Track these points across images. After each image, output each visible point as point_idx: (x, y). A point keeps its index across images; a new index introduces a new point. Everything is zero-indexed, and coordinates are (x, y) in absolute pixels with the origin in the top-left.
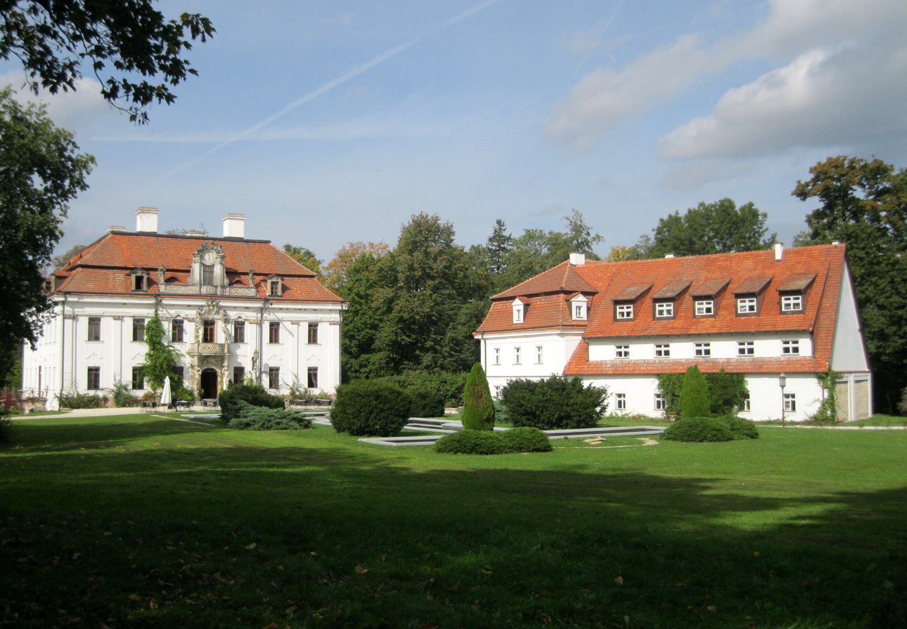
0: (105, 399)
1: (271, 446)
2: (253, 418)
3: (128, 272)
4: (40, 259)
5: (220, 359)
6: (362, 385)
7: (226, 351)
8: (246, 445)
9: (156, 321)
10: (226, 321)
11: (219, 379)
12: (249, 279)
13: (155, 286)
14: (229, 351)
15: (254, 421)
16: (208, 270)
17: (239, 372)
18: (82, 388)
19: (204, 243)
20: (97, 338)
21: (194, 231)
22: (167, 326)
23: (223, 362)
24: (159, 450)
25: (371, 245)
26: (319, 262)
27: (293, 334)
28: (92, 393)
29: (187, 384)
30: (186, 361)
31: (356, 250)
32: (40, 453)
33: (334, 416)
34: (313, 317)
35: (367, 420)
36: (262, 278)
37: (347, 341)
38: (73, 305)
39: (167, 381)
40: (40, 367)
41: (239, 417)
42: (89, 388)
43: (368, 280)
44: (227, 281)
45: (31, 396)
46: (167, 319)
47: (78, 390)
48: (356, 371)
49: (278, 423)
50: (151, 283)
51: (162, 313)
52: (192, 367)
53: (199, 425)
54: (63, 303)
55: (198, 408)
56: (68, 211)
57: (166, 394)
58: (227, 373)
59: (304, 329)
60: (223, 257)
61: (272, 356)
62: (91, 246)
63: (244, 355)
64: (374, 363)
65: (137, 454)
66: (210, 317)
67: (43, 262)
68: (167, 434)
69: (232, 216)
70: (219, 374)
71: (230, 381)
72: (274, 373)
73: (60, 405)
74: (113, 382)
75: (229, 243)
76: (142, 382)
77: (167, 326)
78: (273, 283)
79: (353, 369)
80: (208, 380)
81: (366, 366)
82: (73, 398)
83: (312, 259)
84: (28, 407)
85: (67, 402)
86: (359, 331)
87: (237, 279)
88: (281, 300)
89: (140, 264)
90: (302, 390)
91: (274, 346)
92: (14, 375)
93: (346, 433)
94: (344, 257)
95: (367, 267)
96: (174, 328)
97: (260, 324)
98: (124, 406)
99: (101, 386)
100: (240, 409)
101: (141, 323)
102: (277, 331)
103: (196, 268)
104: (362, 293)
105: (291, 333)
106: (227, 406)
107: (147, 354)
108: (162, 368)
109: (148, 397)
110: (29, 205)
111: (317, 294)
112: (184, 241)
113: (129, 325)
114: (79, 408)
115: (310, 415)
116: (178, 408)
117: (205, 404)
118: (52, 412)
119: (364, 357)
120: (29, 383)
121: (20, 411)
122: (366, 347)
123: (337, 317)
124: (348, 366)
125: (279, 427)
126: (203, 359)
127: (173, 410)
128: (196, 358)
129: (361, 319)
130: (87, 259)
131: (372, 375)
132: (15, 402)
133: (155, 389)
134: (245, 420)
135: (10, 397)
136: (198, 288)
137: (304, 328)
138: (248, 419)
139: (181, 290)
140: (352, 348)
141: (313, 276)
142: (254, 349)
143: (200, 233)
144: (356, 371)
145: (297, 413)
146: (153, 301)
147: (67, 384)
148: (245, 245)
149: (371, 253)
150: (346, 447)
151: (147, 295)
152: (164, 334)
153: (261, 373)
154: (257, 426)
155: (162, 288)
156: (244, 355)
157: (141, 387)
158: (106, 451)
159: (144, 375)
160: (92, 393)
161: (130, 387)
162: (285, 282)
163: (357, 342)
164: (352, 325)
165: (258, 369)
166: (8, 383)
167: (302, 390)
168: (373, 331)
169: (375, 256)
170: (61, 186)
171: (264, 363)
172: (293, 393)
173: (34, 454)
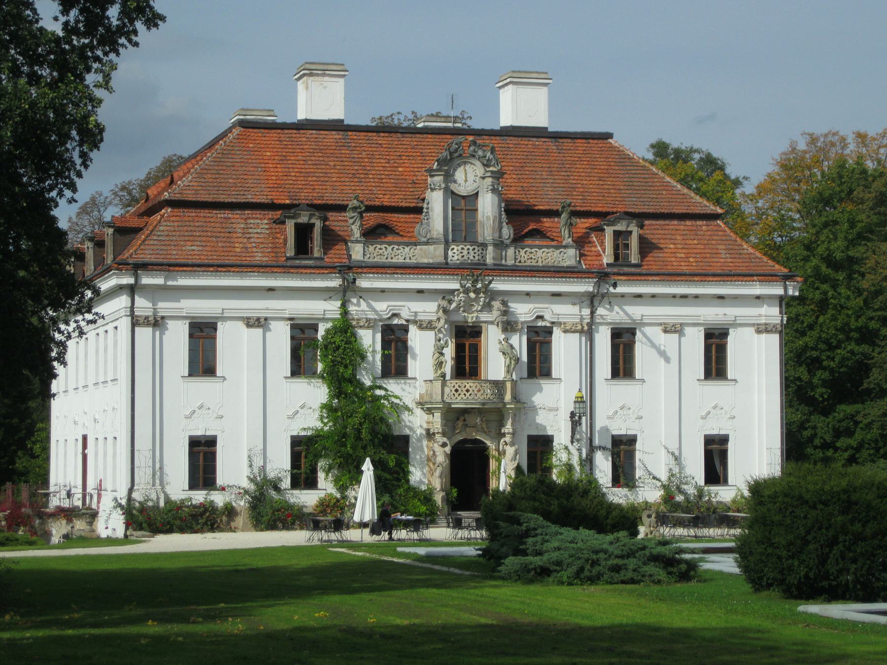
0: (230, 512)
1: (586, 623)
2: (555, 555)
3: (278, 214)
4: (51, 188)
5: (493, 415)
6: (836, 476)
7: (508, 397)
8: (527, 620)
9: (345, 328)
10: (509, 326)
11: (493, 464)
12: (559, 225)
13: (340, 246)
14: (515, 398)
15: (559, 563)
16: (463, 206)
17: (540, 446)
18: (177, 486)
19: (457, 141)
20: (209, 370)
21: (437, 116)
22: (370, 341)
23: (501, 424)
24: (324, 628)
25: (861, 137)
26: (737, 183)
27: (668, 359)
28: (199, 497)
29: (417, 475)
30: (416, 422)
31: (824, 150)
32: (55, 632)
33: (742, 550)
34: (714, 314)
35: (823, 560)
36: (591, 222)
37: (802, 372)
38: (154, 292)
39: (368, 467)
40: (85, 438)
41: (524, 553)
42: (193, 486)
43: (852, 224)
44: (507, 232)
45: (66, 504)
46: (370, 324)
47: (168, 489)
48: (825, 446)
49: (616, 569)
50: (331, 239)
51: (358, 308)
52: (430, 435)
53: (438, 571)
54: (132, 290)
55: (440, 532)
56: (114, 74)
57: (364, 500)
58: (510, 451)
59: (694, 344)
60: (498, 176)
61: (617, 408)
62: (194, 156)
63: (551, 407)
64: (869, 426)
65: (272, 636)
66: (471, 318)
67: (61, 194)
68: (353, 591)
69: (520, 77)
70: (493, 452)
71: (518, 469)
72: (623, 449)
73: (128, 525)
74: (246, 472)
75: (514, 140)
76: (314, 471)
77: (370, 341)
78: (617, 234)
79: (817, 442)
80: (468, 466)
81: (850, 433)
82: (156, 507)
83: (717, 175)
84: (58, 530)
85: (143, 518)
86: (831, 348)
87: (532, 226)
88: (639, 275)
89: (304, 196)
90: (691, 490)
91: (623, 387)
92: (33, 456)
93: (775, 593)
94: (792, 167)
95: (851, 191)
96: (386, 344)
97: (588, 332)
98: (272, 526)
99: (220, 481)
100: (527, 534)
101: (309, 333)
102: (629, 348)
103: (436, 202)
104: (838, 255)
105: (663, 354)
106: (497, 527)
107: (324, 406)
108: (358, 438)
109: (325, 505)
110: (31, 66)
111: (723, 260)
112: (407, 140)
113: (280, 338)
114: (169, 531)
115: (693, 551)
116: (396, 535)
117: (458, 524)
118: (111, 541)
119: (845, 409)
120: (63, 472)
121: (42, 538)
122: (849, 385)
123: (772, 314)
124: (807, 433)
125: (616, 577)
126: (455, 417)
127: (385, 536)
128: (438, 415)
129: (834, 319)
130: (186, 186)
131: (865, 453)
132: (31, 514)
133: (342, 489)
134: (537, 561)
135: (17, 505)
136: (441, 248)
137: (695, 341)
138: (546, 557)
139: (402, 254)
140: (813, 388)
141: (715, 217)
142: (575, 393)
143: (447, 118)
144: (825, 446)
145: (664, 543)
146: (335, 282)
147: (143, 476)
148: (551, 144)
149: (860, 157)
150: (767, 624)
151: (323, 269)
152: (363, 357)
153: (592, 449)
154: (564, 575)
155: (357, 252)
156: (551, 407)
157: (311, 483)
158: (202, 628)
159: (317, 456)
160: (199, 497)
161: (286, 483)
162: (647, 232)
163: (826, 375)
164: (815, 333)
165: (584, 441)
166: (23, 475)
167: (691, 490)
168: (865, 348)
169: (870, 165)
170: (103, 18)
171: (599, 424)
172: (668, 498)
173: (41, 633)
